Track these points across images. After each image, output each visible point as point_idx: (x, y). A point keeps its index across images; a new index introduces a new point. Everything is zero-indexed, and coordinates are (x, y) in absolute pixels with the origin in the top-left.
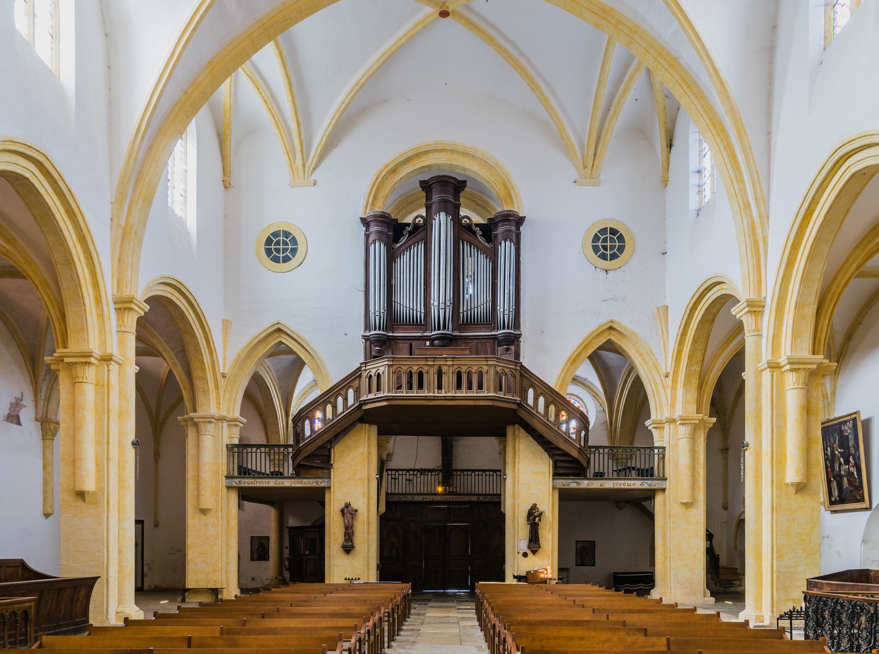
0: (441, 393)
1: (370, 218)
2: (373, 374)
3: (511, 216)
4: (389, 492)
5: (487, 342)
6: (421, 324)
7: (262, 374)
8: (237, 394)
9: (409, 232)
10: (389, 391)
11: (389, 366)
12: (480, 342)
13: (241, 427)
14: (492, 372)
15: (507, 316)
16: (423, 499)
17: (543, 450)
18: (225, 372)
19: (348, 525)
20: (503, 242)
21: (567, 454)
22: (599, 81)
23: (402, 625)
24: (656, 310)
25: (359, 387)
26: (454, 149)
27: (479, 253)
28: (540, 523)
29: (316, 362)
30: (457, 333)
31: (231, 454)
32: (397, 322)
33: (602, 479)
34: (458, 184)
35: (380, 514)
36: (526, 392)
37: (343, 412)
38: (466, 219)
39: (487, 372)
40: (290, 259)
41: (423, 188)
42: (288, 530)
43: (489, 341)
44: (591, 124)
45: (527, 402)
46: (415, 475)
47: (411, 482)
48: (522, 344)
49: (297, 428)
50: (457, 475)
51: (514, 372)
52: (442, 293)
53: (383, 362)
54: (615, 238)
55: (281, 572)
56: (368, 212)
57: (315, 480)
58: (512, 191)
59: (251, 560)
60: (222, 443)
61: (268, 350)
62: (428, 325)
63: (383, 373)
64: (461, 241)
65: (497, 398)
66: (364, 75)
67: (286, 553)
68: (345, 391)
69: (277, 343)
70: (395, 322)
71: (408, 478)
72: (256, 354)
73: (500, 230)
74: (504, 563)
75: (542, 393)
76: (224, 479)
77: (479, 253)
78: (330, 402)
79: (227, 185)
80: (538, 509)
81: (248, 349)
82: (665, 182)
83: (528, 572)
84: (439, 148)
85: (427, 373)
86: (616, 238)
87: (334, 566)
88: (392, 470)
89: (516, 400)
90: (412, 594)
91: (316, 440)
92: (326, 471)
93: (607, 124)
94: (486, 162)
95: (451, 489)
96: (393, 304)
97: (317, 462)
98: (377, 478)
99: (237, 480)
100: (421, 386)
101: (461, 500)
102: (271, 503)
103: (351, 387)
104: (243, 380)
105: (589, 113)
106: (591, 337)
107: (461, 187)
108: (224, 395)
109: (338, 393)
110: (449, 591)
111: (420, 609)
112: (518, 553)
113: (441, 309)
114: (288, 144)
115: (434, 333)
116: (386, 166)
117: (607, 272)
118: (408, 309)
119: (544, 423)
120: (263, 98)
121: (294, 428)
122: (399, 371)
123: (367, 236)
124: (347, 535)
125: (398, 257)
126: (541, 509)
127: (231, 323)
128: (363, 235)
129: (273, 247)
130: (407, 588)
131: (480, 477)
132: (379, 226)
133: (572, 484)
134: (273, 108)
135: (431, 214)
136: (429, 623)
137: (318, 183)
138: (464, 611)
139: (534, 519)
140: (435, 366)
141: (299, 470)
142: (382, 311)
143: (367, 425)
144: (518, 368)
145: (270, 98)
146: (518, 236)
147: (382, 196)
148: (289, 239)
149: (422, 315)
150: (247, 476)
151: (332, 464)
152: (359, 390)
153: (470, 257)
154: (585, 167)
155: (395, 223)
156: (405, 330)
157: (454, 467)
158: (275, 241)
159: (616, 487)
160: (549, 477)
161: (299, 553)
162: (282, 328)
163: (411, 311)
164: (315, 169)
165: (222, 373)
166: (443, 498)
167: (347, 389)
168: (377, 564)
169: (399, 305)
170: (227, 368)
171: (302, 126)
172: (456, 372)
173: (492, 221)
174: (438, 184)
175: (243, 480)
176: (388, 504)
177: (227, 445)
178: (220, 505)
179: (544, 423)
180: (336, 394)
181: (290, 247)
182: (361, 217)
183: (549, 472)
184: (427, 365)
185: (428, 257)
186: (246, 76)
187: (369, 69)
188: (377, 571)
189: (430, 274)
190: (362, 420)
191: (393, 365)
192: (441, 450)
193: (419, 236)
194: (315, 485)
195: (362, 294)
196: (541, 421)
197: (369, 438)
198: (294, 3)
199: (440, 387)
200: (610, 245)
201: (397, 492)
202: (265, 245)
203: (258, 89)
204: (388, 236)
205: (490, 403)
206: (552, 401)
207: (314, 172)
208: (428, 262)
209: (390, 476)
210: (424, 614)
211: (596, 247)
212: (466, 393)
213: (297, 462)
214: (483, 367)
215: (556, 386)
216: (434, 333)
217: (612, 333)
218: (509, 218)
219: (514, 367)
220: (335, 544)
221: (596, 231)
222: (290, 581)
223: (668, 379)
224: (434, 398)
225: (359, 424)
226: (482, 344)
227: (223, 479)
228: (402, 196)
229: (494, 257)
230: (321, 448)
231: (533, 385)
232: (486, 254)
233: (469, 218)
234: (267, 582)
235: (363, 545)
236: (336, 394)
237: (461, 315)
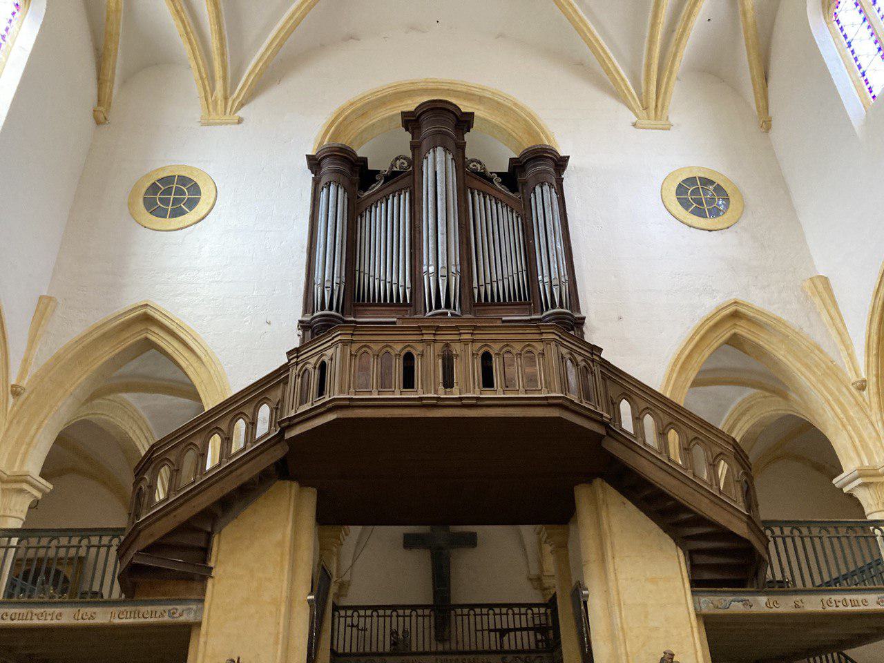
0: (452, 393)
4: (340, 650)
8: (38, 429)
24: (807, 284)
25: (282, 401)
27: (499, 205)
32: (363, 300)
52: (442, 243)
57: (170, 607)
63: (331, 359)
64: (469, 190)
68: (251, 410)
69: (138, 341)
70: (358, 300)
75: (647, 408)
77: (499, 205)
78: (218, 430)
79: (100, 120)
82: (766, 125)
88: (346, 608)
91: (176, 509)
95: (447, 647)
96: (357, 275)
97: (174, 562)
103: (266, 401)
104: (60, 404)
106: (706, 327)
125: (366, 210)
133: (733, 604)
134: (183, 11)
140: (437, 345)
152: (282, 407)
155: (362, 164)
159: (829, 609)
164: (242, 105)
167: (256, 406)
170: (27, 378)
173: (518, 162)
180: (233, 414)
189: (421, 233)
190: (282, 471)
192: (430, 574)
194: (166, 619)
196: (655, 461)
213: (126, 561)
223: (865, 393)
230: (186, 527)
236: (233, 414)
237: (476, 291)
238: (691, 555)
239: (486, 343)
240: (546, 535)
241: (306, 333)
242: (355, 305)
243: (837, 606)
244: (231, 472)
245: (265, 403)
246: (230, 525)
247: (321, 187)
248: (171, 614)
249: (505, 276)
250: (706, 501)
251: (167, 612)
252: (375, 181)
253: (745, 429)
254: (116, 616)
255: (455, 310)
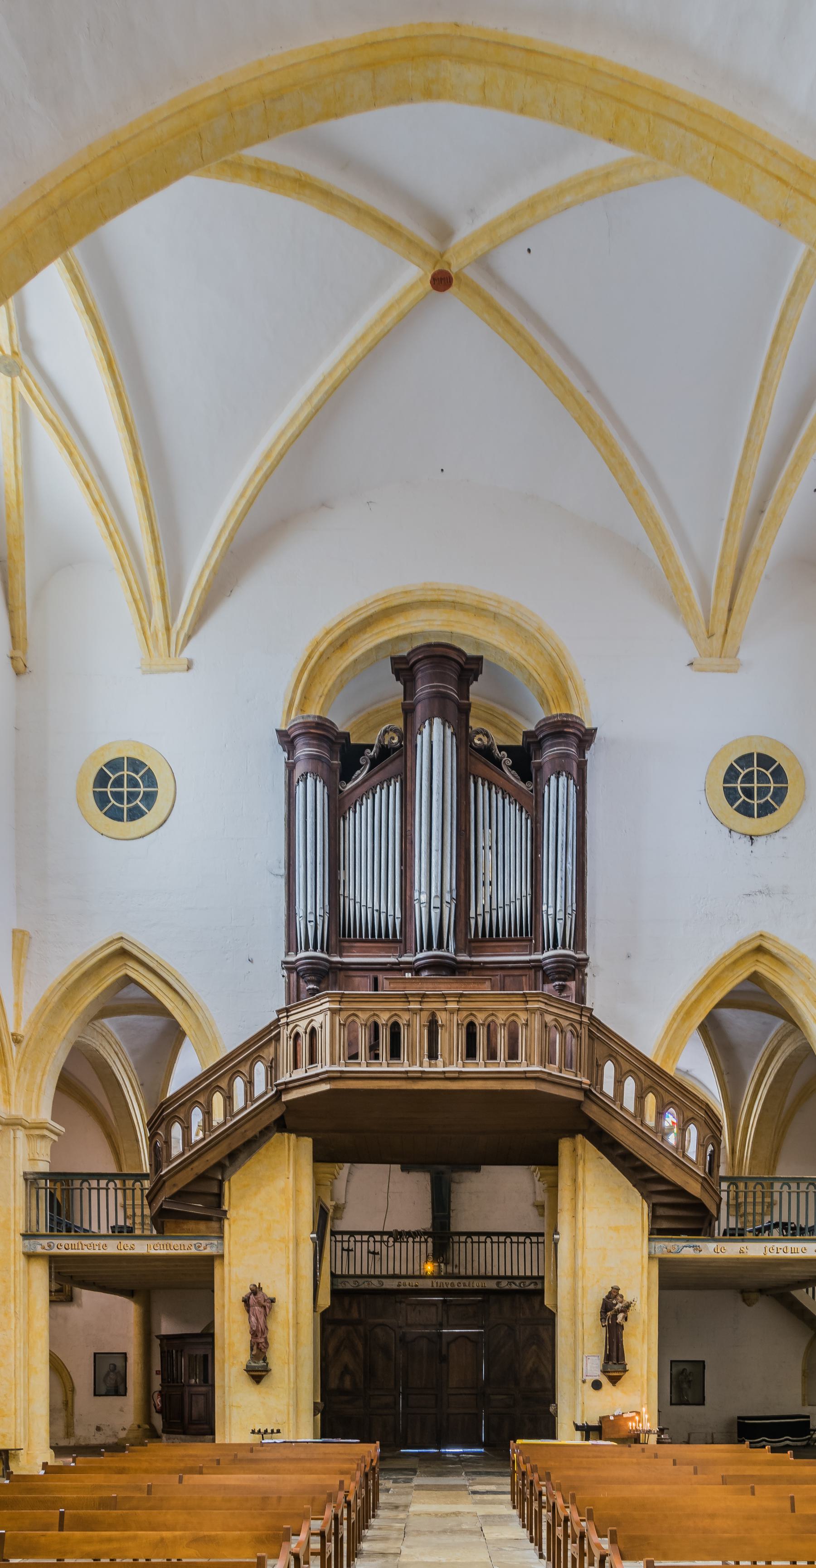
0: (436, 1066)
1: (295, 730)
2: (301, 1030)
3: (569, 727)
4: (339, 1272)
5: (522, 976)
6: (394, 941)
7: (105, 1056)
8: (43, 1075)
9: (370, 759)
10: (333, 1063)
11: (334, 1012)
12: (509, 976)
13: (55, 1141)
14: (536, 1024)
15: (562, 922)
16: (399, 1285)
17: (630, 1185)
18: (19, 1033)
19: (257, 1327)
20: (553, 778)
21: (680, 1192)
22: (748, 441)
23: (360, 1539)
25: (275, 1060)
26: (458, 600)
27: (507, 801)
28: (625, 1324)
29: (195, 1015)
30: (464, 957)
31: (34, 1192)
32: (349, 936)
33: (743, 1241)
34: (465, 663)
35: (320, 1310)
36: (600, 1067)
37: (245, 1108)
38: (481, 736)
39: (527, 1025)
40: (142, 814)
41: (397, 674)
42: (158, 1341)
43: (526, 972)
44: (726, 541)
45: (601, 1088)
46: (384, 1242)
47: (377, 1257)
48: (588, 979)
49: (157, 1139)
50: (459, 1242)
51: (578, 1026)
53: (321, 1004)
54: (768, 773)
55: (147, 1418)
56: (293, 717)
58: (569, 682)
59: (95, 1395)
60: (15, 1170)
61: (101, 994)
62: (408, 942)
64: (472, 778)
65: (545, 1076)
66: (283, 433)
67: (157, 1382)
70: (344, 935)
71: (372, 1250)
72: (79, 1001)
73: (550, 752)
74: (553, 1399)
75: (630, 1071)
76: (19, 1239)
77: (507, 801)
78: (220, 1088)
79: (20, 669)
80: (622, 1297)
81: (64, 988)
83: (603, 1419)
84: (429, 598)
85: (408, 1025)
86: (771, 774)
87: (231, 1406)
88: (343, 1233)
89: (581, 1083)
90: (381, 1458)
91: (193, 1162)
92: (215, 1225)
93: (756, 542)
94: (518, 625)
95: (450, 1269)
97: (197, 1207)
98: (312, 1239)
99: (45, 1242)
100: (395, 1053)
101: (468, 1288)
102: (129, 1293)
105: (723, 520)
106: (722, 967)
107: (471, 670)
108: (18, 1077)
109: (235, 1070)
110: (447, 1450)
111: (399, 1494)
112: (584, 1382)
113: (434, 908)
114: (136, 583)
115: (420, 955)
116: (327, 633)
117: (752, 839)
118: (369, 911)
119: (635, 1130)
120: (82, 476)
121: (151, 1139)
122: (354, 1021)
123: (290, 768)
124: (255, 1347)
126: (628, 1298)
127: (30, 938)
128: (283, 765)
129: (109, 790)
130: (373, 1449)
131: (502, 1246)
132: (318, 746)
134: (103, 501)
135: (413, 724)
136: (419, 1533)
137: (195, 667)
138: (485, 1497)
139: (615, 1317)
141: (163, 1223)
142: (319, 912)
143: (293, 1136)
144: (585, 1019)
145: (97, 479)
146: (582, 767)
147: (320, 694)
148: (141, 774)
149: (398, 922)
150: (64, 1233)
151: (225, 1212)
152: (276, 1065)
153: (490, 828)
154: (710, 636)
155: (344, 741)
156: (364, 952)
157: (453, 1229)
158: (113, 777)
159: (769, 1255)
160: (643, 1240)
161: (178, 1382)
162: (128, 947)
163: (376, 914)
164: (189, 637)
165: (13, 1035)
166: (435, 1285)
167: (252, 1064)
168: (315, 1403)
169: (352, 903)
171: (161, 543)
172: (465, 1024)
174: (426, 661)
175: (56, 1242)
176: (335, 1293)
177: (25, 1174)
178: (12, 1289)
179: (635, 1130)
181: (142, 789)
182: (279, 728)
183: (643, 1228)
184: (408, 1010)
185: (409, 808)
186: (43, 419)
187: (292, 420)
188: (315, 1415)
189: (412, 843)
190: (281, 1125)
191: (340, 1010)
192: (430, 1199)
193: (392, 768)
194: (193, 1251)
195: (282, 882)
196: (628, 1124)
197: (296, 1162)
198: (114, 147)
199: (433, 1055)
200: (759, 788)
201: (352, 1272)
202: (94, 787)
203: (71, 454)
204: (331, 768)
205: (531, 1086)
206: (651, 1087)
207: (186, 644)
208: (409, 819)
209: (339, 1245)
210: (407, 1506)
211: (731, 791)
212: (485, 1067)
213: (157, 1206)
214: (519, 1013)
215: (656, 1054)
216: (420, 955)
217: (760, 960)
218: (566, 730)
219: (577, 1017)
220: (233, 1364)
221: (731, 759)
222: (163, 1431)
224: (423, 1077)
225: (277, 1135)
226: (512, 978)
227: (17, 1239)
228: (359, 712)
229: (536, 810)
230: (202, 1177)
231: (614, 1055)
232: (520, 804)
233: (487, 735)
234: (122, 1435)
235: (286, 1366)
238: (654, 1208)
239: (471, 1012)
240: (539, 1175)
241: (292, 975)
242: (341, 941)
243: (777, 1253)
244: (236, 1129)
245: (260, 1061)
246: (238, 1173)
247: (296, 780)
248: (197, 1247)
249: (507, 902)
250: (669, 1163)
251: (193, 1246)
252: (359, 766)
253: (787, 1053)
254: (152, 1247)
255: (448, 951)
